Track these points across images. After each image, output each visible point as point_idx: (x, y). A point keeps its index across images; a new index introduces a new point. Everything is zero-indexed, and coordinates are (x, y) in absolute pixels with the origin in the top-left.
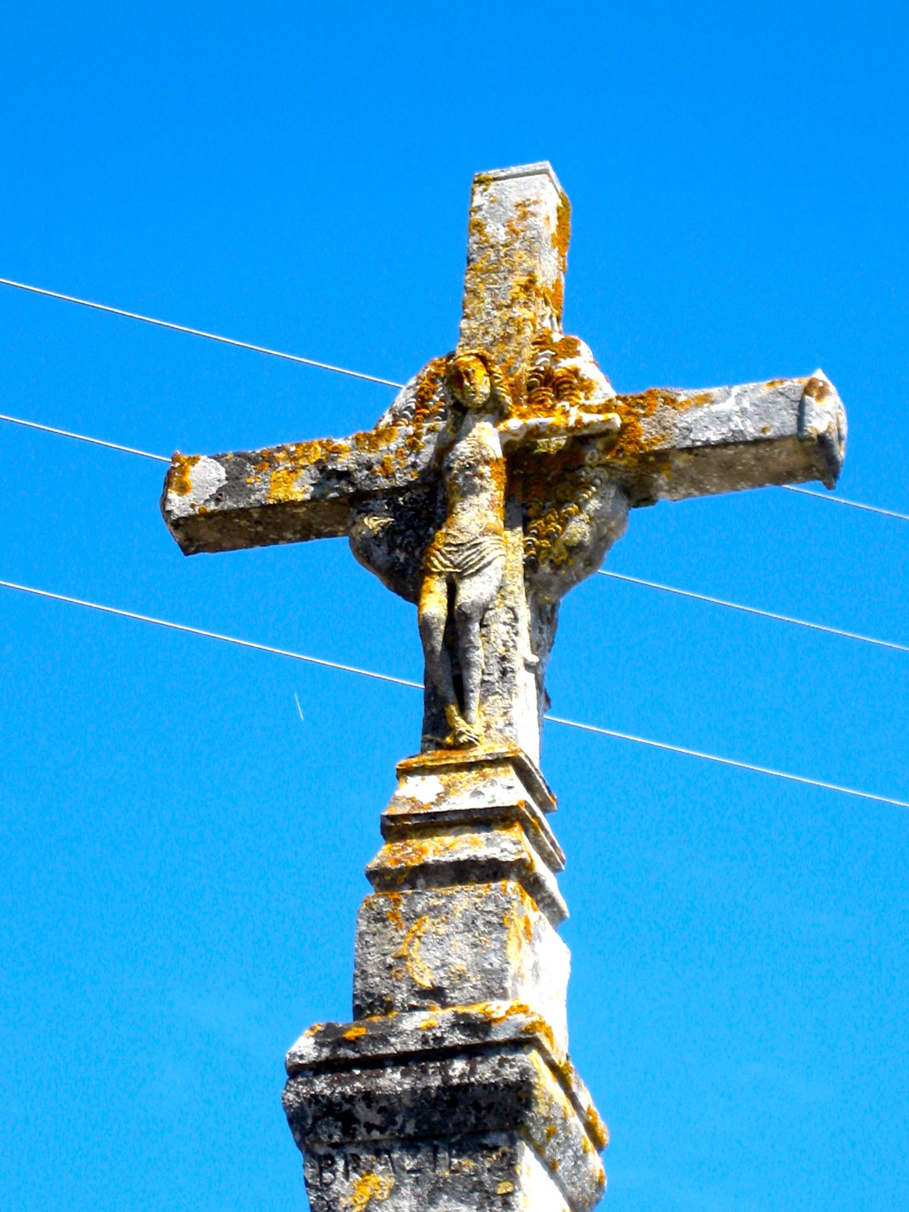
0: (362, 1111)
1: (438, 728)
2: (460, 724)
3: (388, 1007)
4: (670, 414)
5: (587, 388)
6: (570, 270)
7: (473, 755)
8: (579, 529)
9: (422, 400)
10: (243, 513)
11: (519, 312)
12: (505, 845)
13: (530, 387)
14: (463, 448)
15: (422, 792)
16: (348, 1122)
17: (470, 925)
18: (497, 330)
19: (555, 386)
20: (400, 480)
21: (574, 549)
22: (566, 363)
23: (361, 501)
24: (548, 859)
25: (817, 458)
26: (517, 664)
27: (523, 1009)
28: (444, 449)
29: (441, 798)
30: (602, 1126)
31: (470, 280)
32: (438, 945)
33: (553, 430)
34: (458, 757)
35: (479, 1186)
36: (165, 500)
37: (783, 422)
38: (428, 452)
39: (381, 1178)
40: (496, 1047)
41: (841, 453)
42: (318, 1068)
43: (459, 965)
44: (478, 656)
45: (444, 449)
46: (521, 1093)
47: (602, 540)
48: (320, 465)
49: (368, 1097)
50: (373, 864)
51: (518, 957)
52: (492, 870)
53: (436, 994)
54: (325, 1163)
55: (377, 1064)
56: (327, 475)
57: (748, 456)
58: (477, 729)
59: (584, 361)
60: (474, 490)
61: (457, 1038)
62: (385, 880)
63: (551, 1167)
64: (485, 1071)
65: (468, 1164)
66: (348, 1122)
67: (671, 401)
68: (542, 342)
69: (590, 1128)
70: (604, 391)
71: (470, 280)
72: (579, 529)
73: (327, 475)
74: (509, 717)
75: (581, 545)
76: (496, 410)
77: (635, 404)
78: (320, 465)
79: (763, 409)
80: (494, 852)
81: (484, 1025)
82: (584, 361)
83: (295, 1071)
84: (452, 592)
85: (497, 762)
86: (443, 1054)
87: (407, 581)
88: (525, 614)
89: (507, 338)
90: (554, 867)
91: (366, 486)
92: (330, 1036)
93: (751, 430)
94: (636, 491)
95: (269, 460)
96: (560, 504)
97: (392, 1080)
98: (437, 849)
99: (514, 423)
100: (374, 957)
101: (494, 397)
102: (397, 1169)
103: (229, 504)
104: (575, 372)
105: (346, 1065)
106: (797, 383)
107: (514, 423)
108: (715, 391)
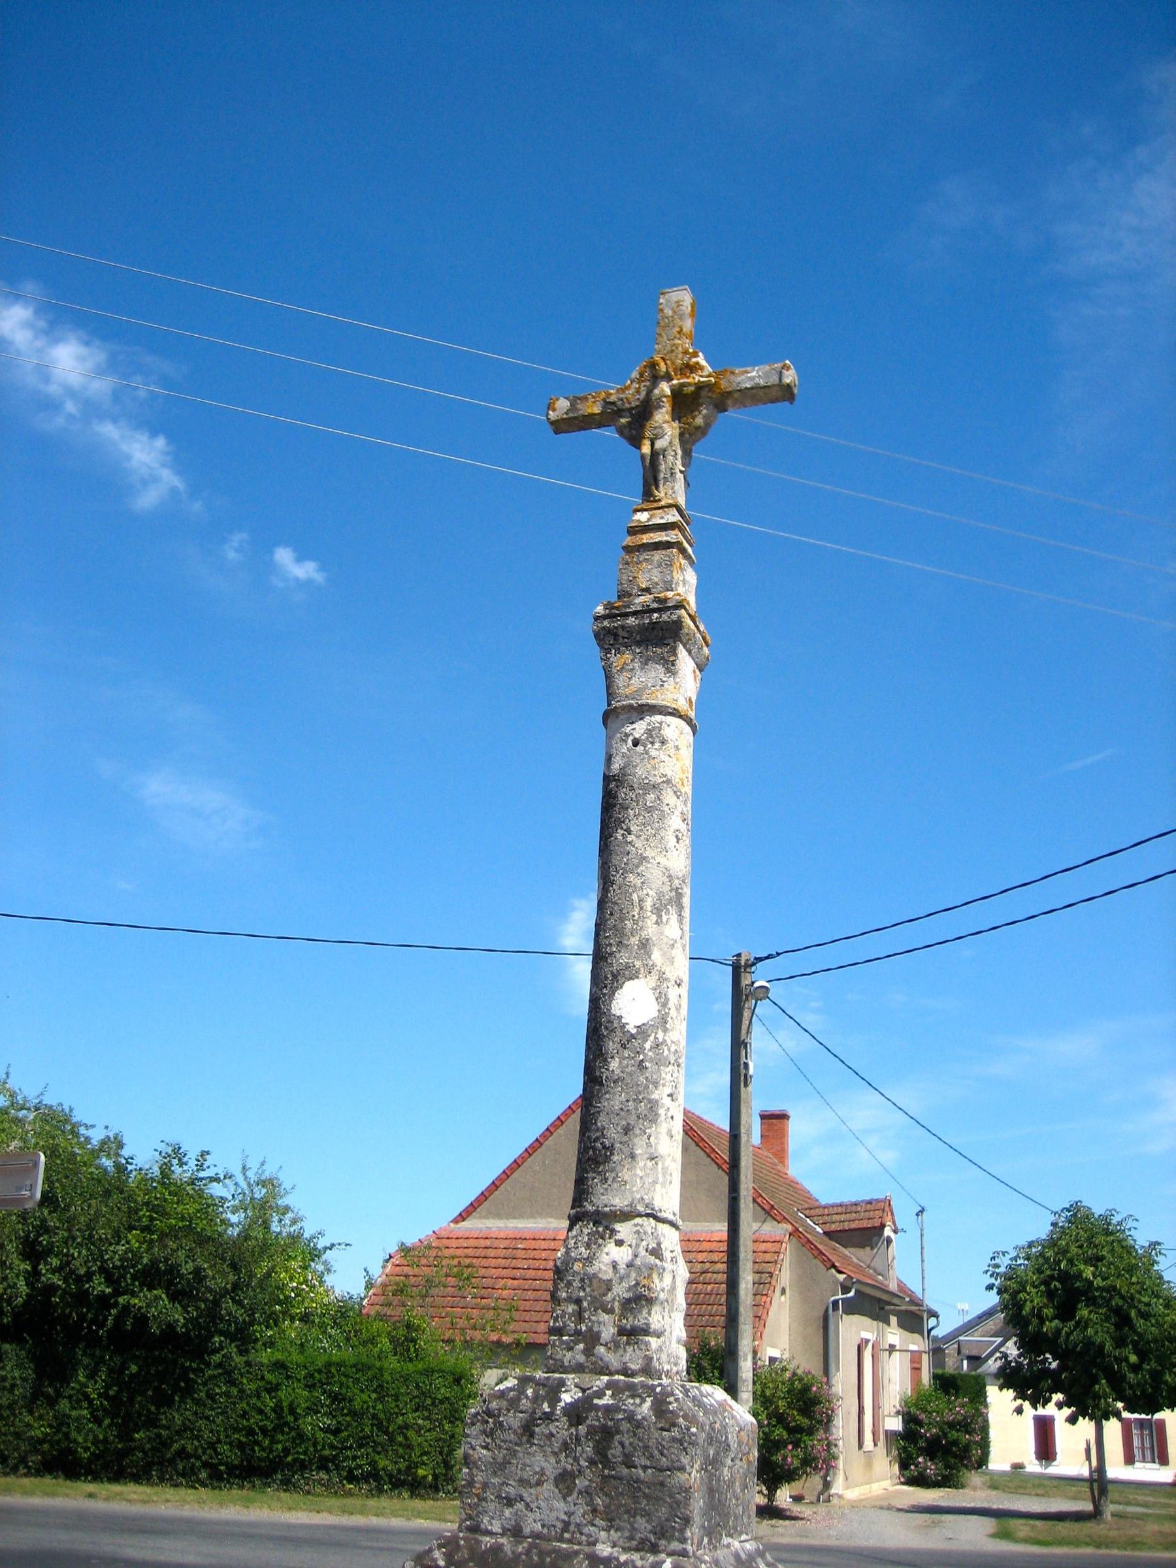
0: (620, 632)
1: (648, 495)
2: (656, 493)
3: (631, 595)
4: (732, 377)
5: (702, 368)
6: (696, 326)
7: (663, 503)
8: (699, 421)
9: (641, 375)
10: (575, 418)
11: (677, 341)
12: (673, 536)
13: (681, 369)
14: (656, 391)
15: (643, 517)
16: (616, 635)
17: (660, 565)
18: (668, 348)
19: (693, 368)
20: (633, 404)
21: (698, 428)
22: (694, 360)
23: (619, 413)
24: (688, 542)
25: (786, 393)
26: (677, 471)
27: (679, 594)
28: (650, 392)
29: (649, 520)
30: (708, 638)
31: (658, 330)
32: (647, 573)
33: (689, 384)
34: (655, 505)
35: (663, 658)
36: (547, 414)
37: (774, 380)
38: (643, 394)
39: (628, 656)
40: (669, 608)
41: (796, 391)
42: (604, 617)
43: (656, 579)
44: (663, 467)
45: (650, 392)
46: (678, 624)
47: (708, 425)
48: (604, 400)
49: (623, 627)
50: (624, 544)
51: (677, 576)
52: (668, 545)
53: (647, 590)
54: (608, 651)
55: (626, 615)
56: (607, 403)
57: (761, 393)
58: (662, 495)
59: (701, 359)
60: (661, 407)
61: (655, 605)
62: (628, 549)
63: (689, 652)
64: (665, 617)
65: (659, 651)
66: (616, 635)
67: (733, 373)
68: (686, 352)
69: (704, 638)
70: (709, 369)
71: (658, 330)
72: (699, 421)
73: (607, 403)
74: (675, 491)
75: (700, 427)
76: (668, 378)
77: (718, 374)
78: (604, 400)
79: (767, 374)
80: (668, 539)
81: (666, 600)
82: (701, 359)
83: (596, 618)
84: (652, 445)
85: (669, 506)
86: (649, 611)
87: (636, 442)
88: (679, 452)
89: (672, 351)
90: (691, 545)
91: (621, 407)
92: (609, 606)
93: (762, 383)
94: (721, 407)
95: (585, 399)
96: (692, 412)
97: (631, 621)
98: (646, 538)
99: (675, 382)
100: (625, 577)
101: (667, 372)
102: (634, 652)
103: (571, 415)
104: (697, 363)
105: (615, 616)
106: (778, 365)
107: (675, 382)
108: (749, 369)
